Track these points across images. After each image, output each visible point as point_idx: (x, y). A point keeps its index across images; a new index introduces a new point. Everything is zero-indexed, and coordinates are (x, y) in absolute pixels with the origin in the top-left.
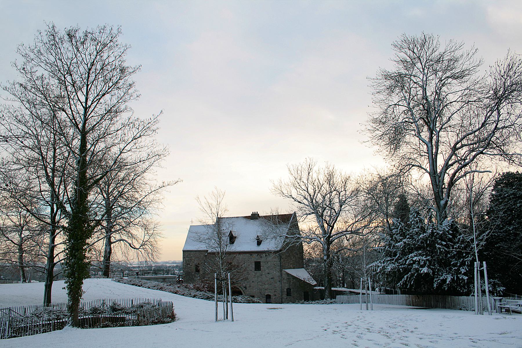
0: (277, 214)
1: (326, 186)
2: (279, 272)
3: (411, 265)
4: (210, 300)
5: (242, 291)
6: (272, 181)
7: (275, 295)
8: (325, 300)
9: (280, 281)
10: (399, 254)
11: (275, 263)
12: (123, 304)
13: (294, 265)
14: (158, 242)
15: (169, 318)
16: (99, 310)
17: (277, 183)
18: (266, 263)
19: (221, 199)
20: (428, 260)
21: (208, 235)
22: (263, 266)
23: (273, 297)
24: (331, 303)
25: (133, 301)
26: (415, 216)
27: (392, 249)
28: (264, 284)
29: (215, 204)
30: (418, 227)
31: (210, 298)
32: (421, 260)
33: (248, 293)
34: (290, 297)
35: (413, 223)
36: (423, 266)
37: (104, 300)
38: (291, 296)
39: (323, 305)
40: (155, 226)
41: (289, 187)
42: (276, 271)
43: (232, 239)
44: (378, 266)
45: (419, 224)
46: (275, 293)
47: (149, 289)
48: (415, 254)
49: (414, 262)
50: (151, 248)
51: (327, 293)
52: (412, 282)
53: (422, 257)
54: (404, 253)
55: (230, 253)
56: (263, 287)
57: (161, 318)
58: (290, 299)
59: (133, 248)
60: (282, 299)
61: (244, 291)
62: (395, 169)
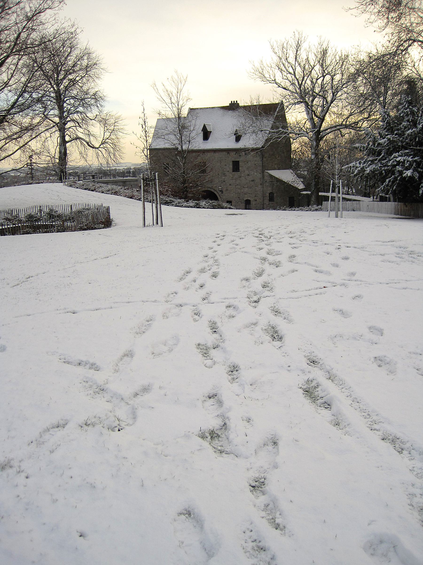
0: (258, 104)
1: (318, 68)
2: (260, 174)
3: (395, 166)
4: (168, 205)
5: (217, 195)
6: (253, 63)
7: (256, 200)
8: (310, 207)
9: (261, 184)
10: (384, 153)
11: (256, 162)
12: (60, 211)
13: (279, 165)
14: (121, 140)
15: (102, 225)
16: (35, 217)
17: (257, 65)
18: (246, 163)
19: (182, 85)
20: (415, 161)
21: (167, 130)
22: (241, 167)
23: (253, 203)
24: (316, 210)
25: (73, 207)
26: (406, 106)
27: (377, 147)
28: (244, 187)
29: (175, 92)
30: (408, 121)
31: (169, 202)
32: (406, 161)
33: (224, 197)
34: (272, 203)
35: (401, 115)
36: (407, 169)
37: (41, 206)
38: (274, 201)
39: (298, 211)
40: (116, 121)
41: (273, 69)
42: (256, 172)
43: (206, 134)
44: (357, 167)
45: (409, 117)
46: (256, 198)
47: (103, 194)
48: (400, 154)
49: (399, 163)
50: (112, 146)
51: (313, 199)
52: (395, 187)
53: (409, 157)
54: (389, 153)
55: (204, 151)
56: (242, 191)
57: (91, 224)
58: (272, 205)
59: (91, 147)
60: (263, 205)
61: (220, 196)
62: (390, 45)
